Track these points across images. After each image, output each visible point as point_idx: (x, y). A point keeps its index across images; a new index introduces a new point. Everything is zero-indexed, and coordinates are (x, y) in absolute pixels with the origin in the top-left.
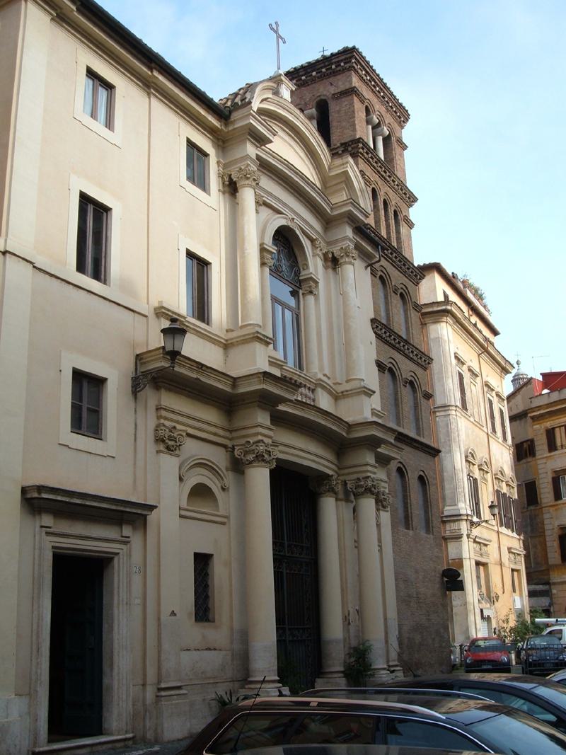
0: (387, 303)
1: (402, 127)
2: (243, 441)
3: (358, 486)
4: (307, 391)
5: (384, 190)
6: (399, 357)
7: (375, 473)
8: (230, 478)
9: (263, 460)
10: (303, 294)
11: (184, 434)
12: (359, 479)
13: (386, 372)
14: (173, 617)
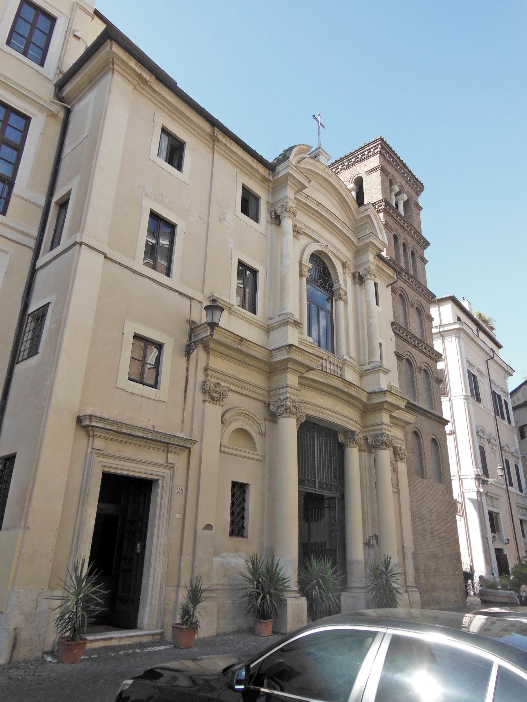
0: (405, 313)
1: (419, 195)
2: (276, 398)
3: (376, 441)
4: (336, 368)
5: (403, 236)
6: (414, 351)
7: (390, 431)
8: (265, 426)
9: (291, 412)
10: (335, 300)
11: (227, 390)
12: (376, 435)
13: (404, 361)
14: (208, 532)
